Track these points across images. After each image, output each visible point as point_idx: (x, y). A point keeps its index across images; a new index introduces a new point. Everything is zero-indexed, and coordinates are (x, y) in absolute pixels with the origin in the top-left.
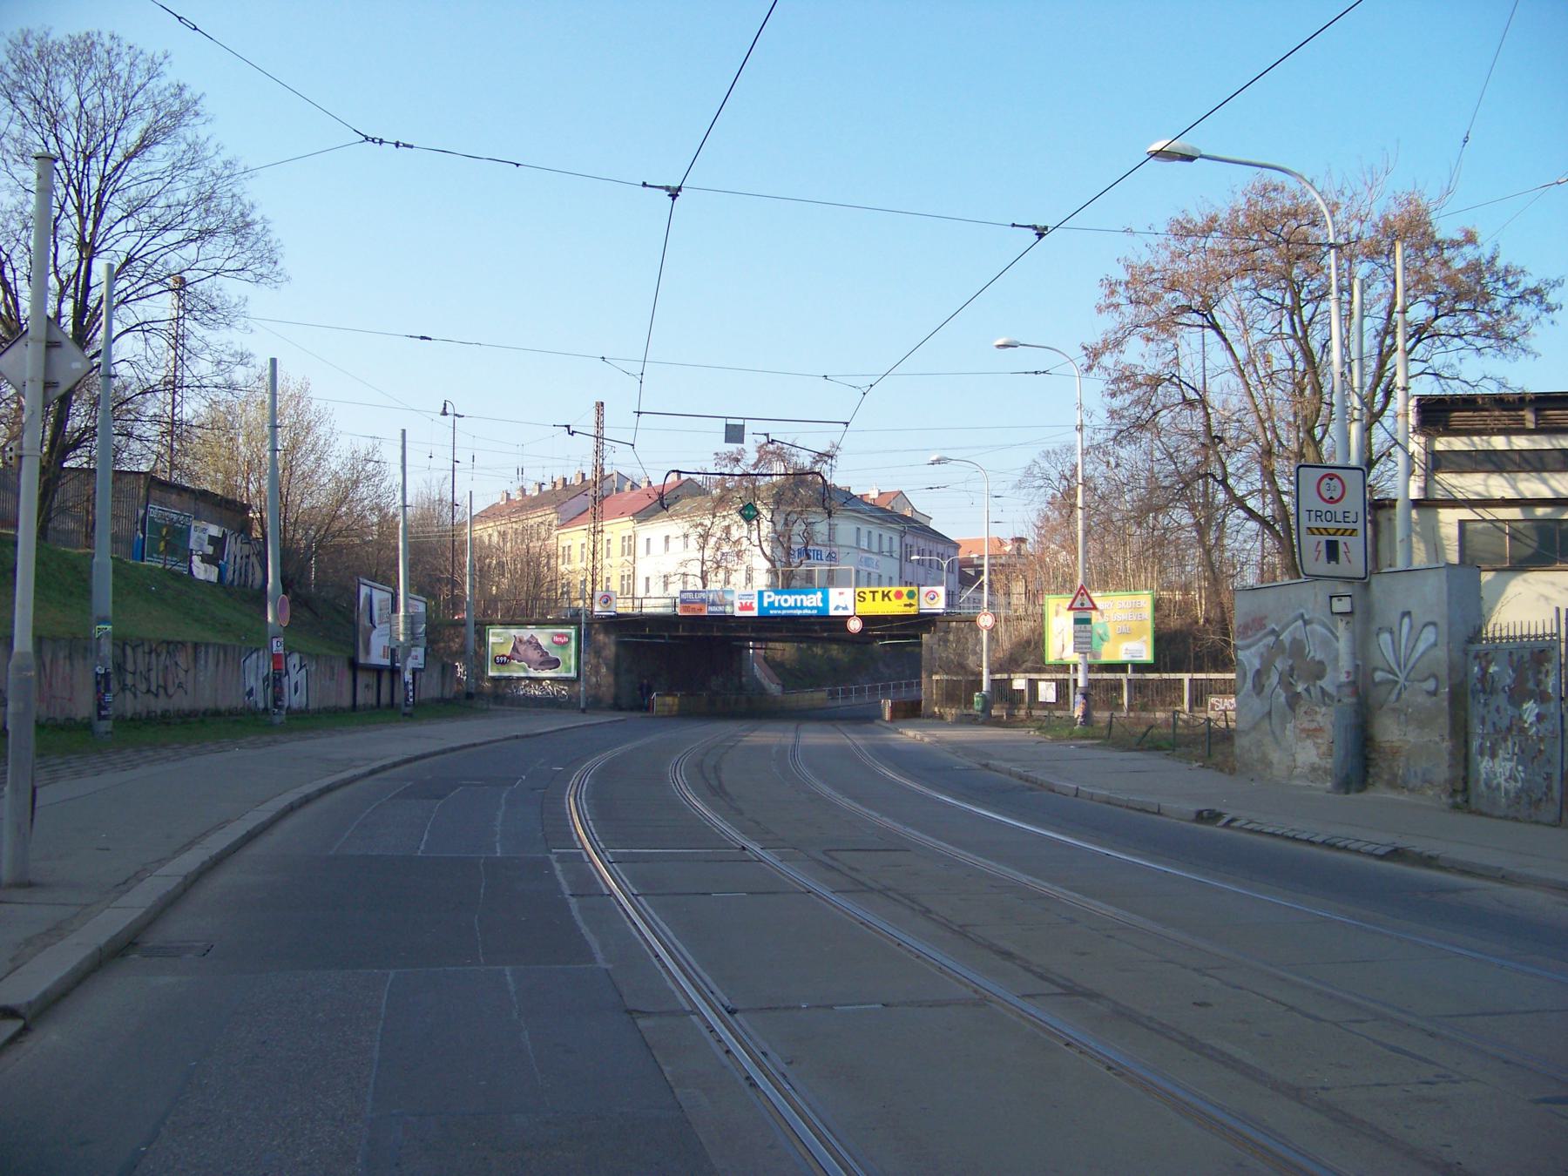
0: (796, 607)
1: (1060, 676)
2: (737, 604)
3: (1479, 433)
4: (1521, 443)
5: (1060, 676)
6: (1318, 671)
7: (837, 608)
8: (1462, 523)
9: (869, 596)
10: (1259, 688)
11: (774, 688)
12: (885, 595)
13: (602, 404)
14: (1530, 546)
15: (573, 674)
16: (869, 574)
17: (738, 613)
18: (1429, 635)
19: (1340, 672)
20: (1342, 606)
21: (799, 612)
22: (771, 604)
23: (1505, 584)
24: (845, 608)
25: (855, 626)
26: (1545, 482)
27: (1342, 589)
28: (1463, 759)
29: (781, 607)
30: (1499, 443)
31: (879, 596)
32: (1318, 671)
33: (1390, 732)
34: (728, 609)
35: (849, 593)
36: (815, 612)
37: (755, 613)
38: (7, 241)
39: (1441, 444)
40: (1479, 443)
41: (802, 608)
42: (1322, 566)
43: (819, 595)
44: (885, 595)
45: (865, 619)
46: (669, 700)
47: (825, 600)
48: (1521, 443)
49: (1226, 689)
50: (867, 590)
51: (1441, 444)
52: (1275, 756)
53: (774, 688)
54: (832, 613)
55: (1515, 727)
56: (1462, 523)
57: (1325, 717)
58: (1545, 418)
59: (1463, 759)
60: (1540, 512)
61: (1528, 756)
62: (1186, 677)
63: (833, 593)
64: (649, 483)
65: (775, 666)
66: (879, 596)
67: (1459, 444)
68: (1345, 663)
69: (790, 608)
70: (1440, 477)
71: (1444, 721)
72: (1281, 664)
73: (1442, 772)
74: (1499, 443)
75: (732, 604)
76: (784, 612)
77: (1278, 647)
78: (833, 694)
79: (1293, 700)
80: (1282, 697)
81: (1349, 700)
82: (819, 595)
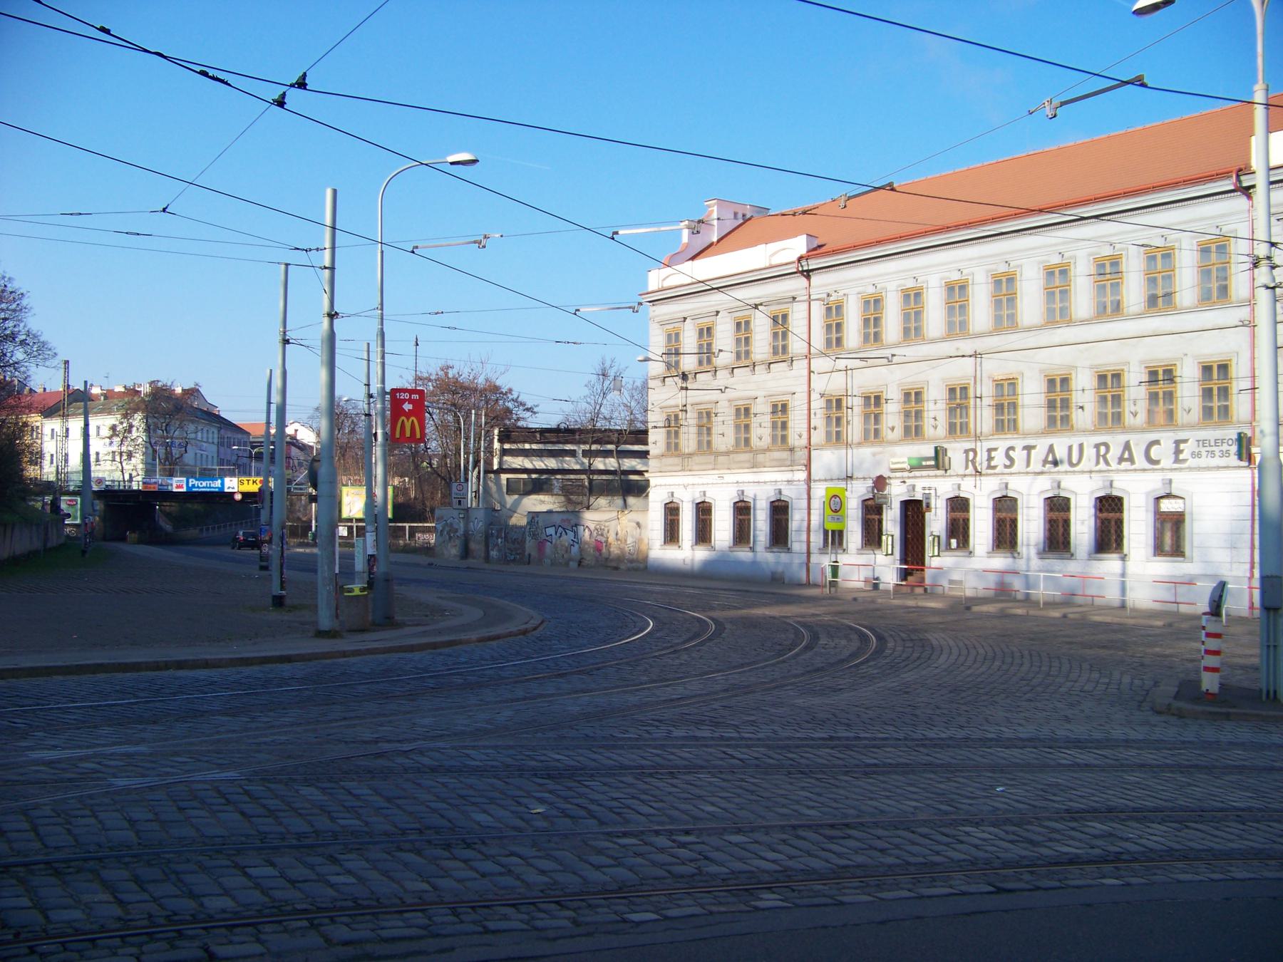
0: (207, 487)
1: (349, 524)
2: (174, 485)
3: (520, 442)
4: (534, 446)
5: (349, 524)
6: (456, 531)
7: (229, 488)
8: (508, 479)
9: (246, 482)
10: (441, 535)
11: (168, 527)
12: (254, 482)
13: (68, 361)
14: (530, 487)
15: (78, 522)
16: (202, 455)
17: (175, 490)
18: (481, 524)
19: (461, 532)
20: (461, 516)
21: (208, 490)
22: (193, 486)
23: (521, 500)
24: (233, 488)
25: (238, 497)
26: (542, 461)
27: (462, 512)
28: (487, 552)
29: (198, 487)
30: (527, 446)
31: (251, 482)
32: (456, 531)
33: (473, 546)
34: (170, 488)
35: (235, 480)
36: (217, 490)
37: (184, 490)
38: (122, 423)
39: (507, 446)
40: (520, 446)
41: (210, 487)
42: (458, 506)
43: (219, 481)
44: (254, 482)
45: (243, 494)
46: (133, 535)
47: (223, 484)
48: (534, 446)
49: (428, 530)
50: (245, 479)
51: (507, 446)
52: (445, 552)
53: (168, 527)
54: (226, 490)
55: (497, 545)
56: (508, 479)
57: (458, 542)
58: (544, 436)
59: (487, 552)
60: (534, 476)
61: (499, 550)
62: (407, 525)
63: (227, 480)
64: (45, 389)
65: (168, 515)
66: (251, 482)
67: (514, 446)
68: (462, 530)
69: (204, 487)
70: (505, 458)
71: (483, 543)
72: (447, 529)
73: (483, 555)
74: (527, 446)
75: (172, 485)
76: (200, 490)
77: (447, 524)
78: (201, 530)
79: (450, 538)
80: (447, 537)
81: (463, 538)
82: (219, 481)
